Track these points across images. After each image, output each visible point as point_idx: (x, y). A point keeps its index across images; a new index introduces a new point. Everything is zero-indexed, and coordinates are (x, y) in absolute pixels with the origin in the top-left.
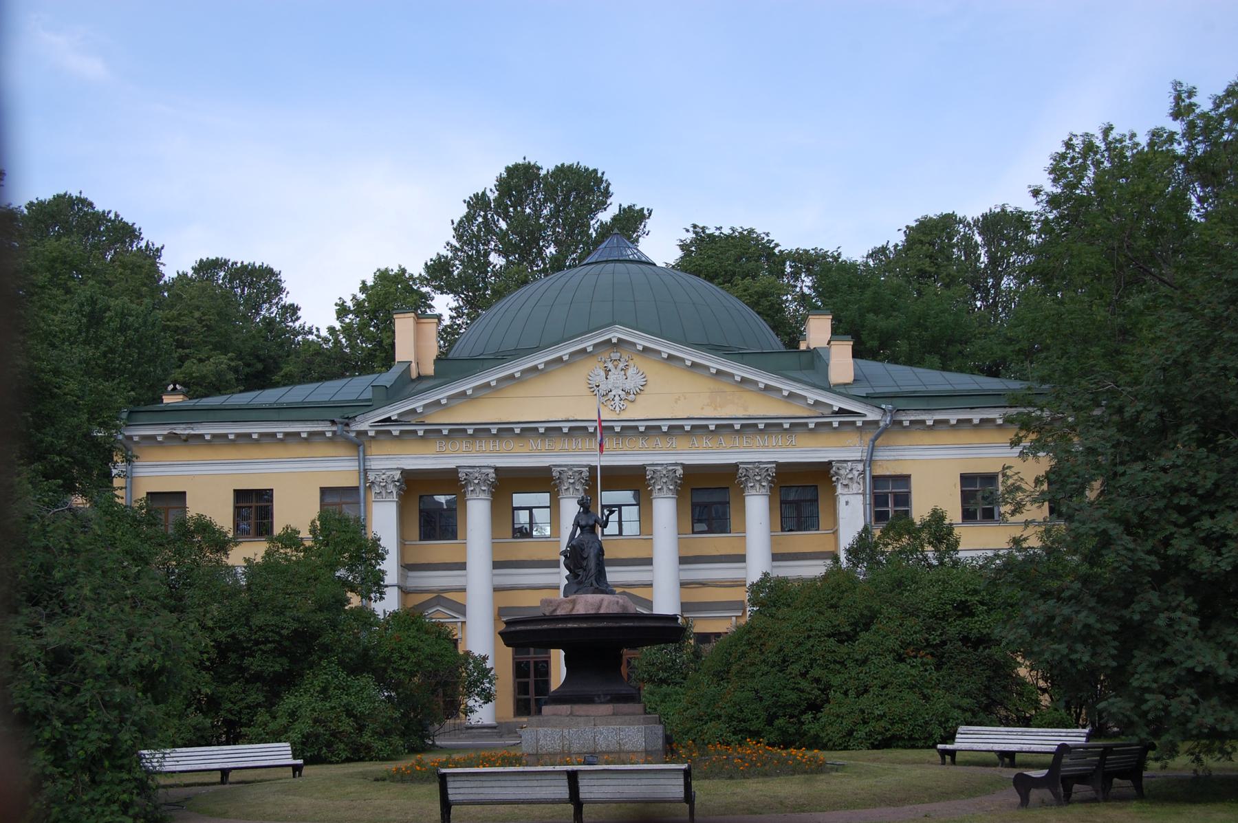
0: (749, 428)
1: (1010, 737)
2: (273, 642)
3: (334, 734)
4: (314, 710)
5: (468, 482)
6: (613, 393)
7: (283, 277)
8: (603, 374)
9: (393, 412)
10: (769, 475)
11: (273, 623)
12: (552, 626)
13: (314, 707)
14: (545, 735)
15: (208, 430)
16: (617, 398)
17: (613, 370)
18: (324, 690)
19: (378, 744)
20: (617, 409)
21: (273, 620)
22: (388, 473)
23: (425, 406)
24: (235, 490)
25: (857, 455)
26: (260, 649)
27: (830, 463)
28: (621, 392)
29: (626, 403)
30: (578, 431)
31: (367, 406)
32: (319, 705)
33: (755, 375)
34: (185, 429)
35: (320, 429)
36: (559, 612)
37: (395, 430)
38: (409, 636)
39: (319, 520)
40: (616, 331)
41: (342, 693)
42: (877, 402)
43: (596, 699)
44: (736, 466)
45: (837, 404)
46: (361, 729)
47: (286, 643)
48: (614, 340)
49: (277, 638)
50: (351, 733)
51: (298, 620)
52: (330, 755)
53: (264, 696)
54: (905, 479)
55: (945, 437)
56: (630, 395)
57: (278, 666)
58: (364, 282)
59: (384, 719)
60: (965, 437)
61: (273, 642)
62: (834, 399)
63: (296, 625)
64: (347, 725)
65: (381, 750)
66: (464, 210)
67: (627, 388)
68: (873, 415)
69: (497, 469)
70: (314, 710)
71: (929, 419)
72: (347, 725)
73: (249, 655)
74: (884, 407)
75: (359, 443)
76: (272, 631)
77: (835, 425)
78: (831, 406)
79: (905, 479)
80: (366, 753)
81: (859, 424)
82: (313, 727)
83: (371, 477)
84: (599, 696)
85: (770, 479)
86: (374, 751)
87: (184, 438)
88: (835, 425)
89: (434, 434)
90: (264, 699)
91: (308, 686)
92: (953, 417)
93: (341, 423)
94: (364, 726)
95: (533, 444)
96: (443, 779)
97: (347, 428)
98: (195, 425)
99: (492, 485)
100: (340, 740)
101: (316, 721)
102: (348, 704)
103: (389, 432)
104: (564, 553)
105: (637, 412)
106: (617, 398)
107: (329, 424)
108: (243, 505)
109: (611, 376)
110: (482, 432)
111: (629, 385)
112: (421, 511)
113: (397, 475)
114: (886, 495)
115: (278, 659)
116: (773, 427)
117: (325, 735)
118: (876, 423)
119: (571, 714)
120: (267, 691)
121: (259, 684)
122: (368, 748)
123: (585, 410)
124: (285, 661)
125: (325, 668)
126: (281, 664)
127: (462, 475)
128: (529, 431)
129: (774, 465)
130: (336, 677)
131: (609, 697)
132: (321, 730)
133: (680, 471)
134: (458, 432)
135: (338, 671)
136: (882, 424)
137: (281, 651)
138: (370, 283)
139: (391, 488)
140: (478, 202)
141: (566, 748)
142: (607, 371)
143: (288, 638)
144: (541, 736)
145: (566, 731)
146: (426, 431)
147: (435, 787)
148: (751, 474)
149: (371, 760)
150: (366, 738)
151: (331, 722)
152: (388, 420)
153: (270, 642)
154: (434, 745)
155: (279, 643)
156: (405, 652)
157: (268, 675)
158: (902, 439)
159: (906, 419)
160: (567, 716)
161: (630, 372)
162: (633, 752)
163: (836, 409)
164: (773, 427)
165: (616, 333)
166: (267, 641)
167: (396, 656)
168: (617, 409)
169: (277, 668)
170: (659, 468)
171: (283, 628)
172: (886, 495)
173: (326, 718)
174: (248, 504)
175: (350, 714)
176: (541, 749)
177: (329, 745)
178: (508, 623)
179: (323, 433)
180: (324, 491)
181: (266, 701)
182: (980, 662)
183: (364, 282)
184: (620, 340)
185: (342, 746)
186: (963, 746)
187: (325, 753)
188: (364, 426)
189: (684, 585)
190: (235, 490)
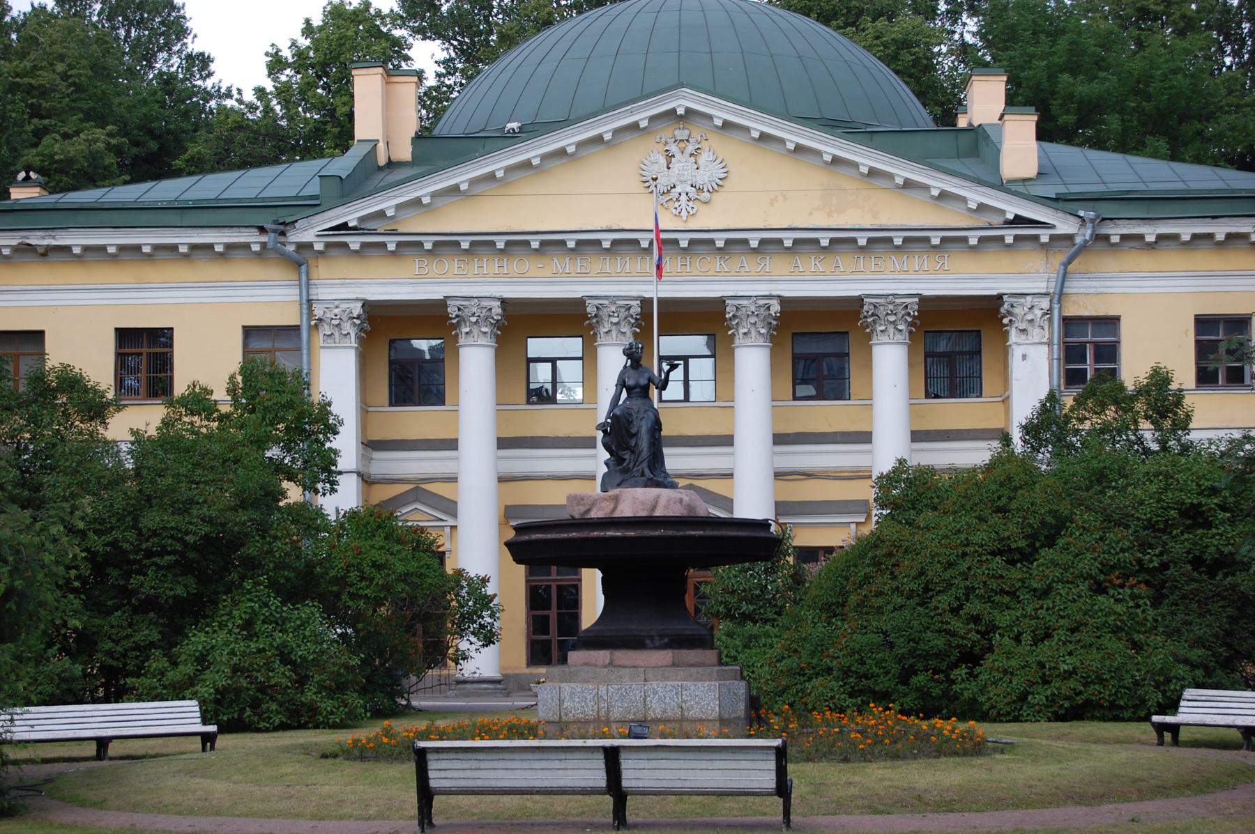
0: (879, 243)
2: (174, 552)
3: (262, 689)
4: (233, 653)
5: (461, 320)
6: (678, 189)
8: (663, 161)
9: (351, 214)
10: (909, 314)
11: (173, 524)
13: (233, 649)
14: (572, 695)
15: (76, 239)
17: (678, 155)
18: (248, 624)
19: (327, 705)
21: (173, 521)
22: (344, 306)
23: (399, 207)
25: (1041, 287)
27: (1000, 297)
28: (689, 189)
29: (697, 205)
31: (312, 206)
32: (240, 646)
34: (43, 238)
35: (242, 240)
36: (595, 514)
37: (354, 242)
40: (683, 98)
42: (1071, 206)
43: (648, 642)
44: (859, 300)
45: (1013, 208)
46: (302, 681)
48: (681, 111)
49: (179, 547)
51: (209, 521)
52: (256, 719)
54: (1112, 322)
56: (702, 193)
57: (180, 588)
58: (308, 22)
59: (336, 669)
60: (1203, 259)
61: (174, 552)
62: (1007, 202)
64: (281, 675)
65: (332, 713)
67: (699, 183)
68: (1065, 226)
70: (233, 653)
71: (1150, 232)
72: (281, 675)
74: (1082, 213)
76: (172, 537)
77: (1009, 240)
78: (1003, 212)
79: (1112, 322)
81: (1044, 239)
82: (231, 678)
83: (318, 311)
84: (652, 638)
85: (909, 319)
86: (321, 714)
87: (41, 250)
88: (1009, 240)
89: (410, 247)
91: (225, 618)
92: (1186, 230)
93: (274, 231)
94: (307, 677)
96: (421, 757)
97: (282, 239)
101: (236, 669)
102: (284, 645)
103: (345, 245)
104: (602, 427)
106: (684, 197)
107: (255, 232)
108: (127, 350)
109: (675, 164)
110: (482, 245)
111: (703, 178)
112: (391, 363)
113: (357, 309)
114: (1082, 346)
115: (180, 579)
116: (916, 242)
117: (248, 689)
118: (1070, 238)
119: (611, 664)
120: (163, 625)
121: (152, 615)
122: (313, 710)
125: (249, 592)
126: (186, 586)
127: (452, 311)
128: (552, 245)
129: (917, 300)
130: (266, 605)
132: (244, 683)
133: (776, 307)
134: (446, 246)
135: (269, 596)
136: (1078, 240)
137: (184, 567)
138: (317, 21)
139: (348, 327)
141: (602, 713)
142: (670, 157)
143: (195, 547)
144: (566, 695)
145: (603, 688)
147: (410, 769)
148: (881, 312)
149: (317, 727)
150: (309, 695)
151: (259, 671)
152: (344, 226)
153: (169, 553)
154: (409, 706)
155: (182, 554)
157: (166, 601)
158: (1107, 263)
159: (1115, 232)
160: (605, 667)
161: (704, 158)
162: (701, 720)
163: (1010, 216)
164: (916, 242)
165: (682, 101)
166: (163, 552)
167: (353, 575)
168: (684, 213)
169: (180, 591)
170: (745, 302)
171: (187, 533)
172: (1082, 346)
173: (251, 664)
176: (566, 714)
178: (518, 529)
179: (247, 246)
180: (249, 331)
183: (308, 22)
185: (274, 707)
190: (116, 329)
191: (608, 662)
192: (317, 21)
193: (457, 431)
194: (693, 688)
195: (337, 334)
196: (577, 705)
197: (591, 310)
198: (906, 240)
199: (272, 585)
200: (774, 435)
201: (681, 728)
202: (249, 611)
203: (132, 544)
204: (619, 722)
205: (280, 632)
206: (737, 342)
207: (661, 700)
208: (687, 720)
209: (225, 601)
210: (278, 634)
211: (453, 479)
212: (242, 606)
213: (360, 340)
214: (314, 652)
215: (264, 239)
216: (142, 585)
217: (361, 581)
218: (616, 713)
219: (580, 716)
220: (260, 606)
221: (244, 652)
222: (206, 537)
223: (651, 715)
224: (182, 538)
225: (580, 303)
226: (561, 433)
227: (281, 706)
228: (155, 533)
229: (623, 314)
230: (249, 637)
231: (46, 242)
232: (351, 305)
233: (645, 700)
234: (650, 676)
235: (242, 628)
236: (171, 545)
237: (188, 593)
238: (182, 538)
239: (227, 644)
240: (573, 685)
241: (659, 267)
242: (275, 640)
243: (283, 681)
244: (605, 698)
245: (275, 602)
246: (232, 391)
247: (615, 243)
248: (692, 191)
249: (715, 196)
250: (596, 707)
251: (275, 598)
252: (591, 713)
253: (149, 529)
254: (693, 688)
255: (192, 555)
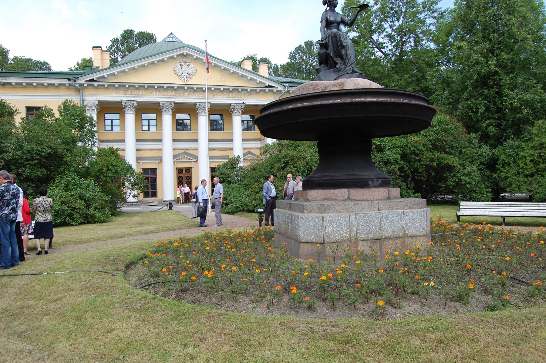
0: (236, 90)
1: (511, 208)
2: (36, 159)
3: (74, 209)
4: (61, 196)
5: (126, 107)
6: (184, 74)
7: (51, 65)
8: (180, 67)
11: (36, 149)
12: (347, 100)
13: (61, 195)
14: (332, 222)
15: (13, 80)
16: (185, 77)
17: (184, 66)
18: (67, 186)
19: (98, 214)
20: (185, 81)
21: (36, 148)
22: (93, 102)
23: (108, 75)
24: (26, 107)
26: (29, 164)
28: (187, 74)
29: (189, 79)
30: (171, 88)
32: (64, 194)
33: (239, 70)
34: (3, 80)
35: (63, 82)
37: (96, 84)
38: (111, 159)
39: (63, 105)
40: (186, 50)
41: (77, 188)
43: (370, 183)
45: (268, 83)
46: (88, 207)
47: (44, 160)
48: (185, 54)
49: (39, 157)
50: (83, 209)
51: (51, 147)
52: (71, 221)
53: (32, 189)
55: (52, 91)
57: (40, 173)
58: (78, 62)
59: (101, 201)
61: (36, 159)
62: (267, 81)
63: (50, 150)
64: (81, 204)
65: (100, 218)
66: (110, 43)
67: (189, 73)
68: (280, 88)
69: (138, 102)
70: (61, 196)
72: (81, 204)
73: (24, 167)
74: (284, 85)
75: (80, 89)
76: (36, 153)
78: (265, 84)
80: (92, 219)
81: (275, 91)
82: (61, 206)
84: (372, 180)
86: (96, 218)
87: (2, 83)
88: (267, 91)
89: (112, 86)
90: (32, 191)
91: (58, 184)
93: (73, 79)
94: (90, 204)
95: (152, 92)
97: (75, 82)
98: (7, 78)
99: (135, 108)
100: (77, 213)
101: (63, 203)
102: (81, 193)
103: (93, 85)
105: (194, 81)
106: (185, 77)
107: (67, 80)
108: (29, 113)
109: (183, 68)
110: (132, 87)
111: (190, 72)
113: (97, 103)
115: (40, 169)
116: (244, 90)
117: (68, 210)
118: (280, 91)
119: (349, 198)
120: (34, 187)
121: (29, 183)
122: (93, 216)
123: (175, 81)
124: (44, 170)
125: (67, 174)
126: (42, 172)
127: (123, 104)
128: (151, 87)
130: (74, 179)
131: (380, 181)
132: (66, 208)
134: (122, 86)
135: (75, 175)
136: (283, 92)
137: (41, 165)
138: (80, 62)
139: (94, 108)
140: (115, 41)
141: (353, 235)
143: (46, 158)
144: (327, 223)
145: (353, 217)
146: (108, 85)
148: (235, 108)
149: (95, 223)
150: (91, 211)
151: (72, 203)
152: (93, 80)
153: (35, 160)
154: (121, 212)
155: (40, 160)
156: (110, 167)
157: (34, 178)
160: (345, 201)
161: (190, 67)
162: (416, 236)
163: (267, 85)
164: (244, 90)
166: (32, 159)
167: (105, 169)
168: (185, 81)
169: (40, 174)
170: (201, 104)
171: (42, 152)
173: (69, 200)
174: (32, 113)
175: (81, 198)
176: (328, 237)
177: (70, 215)
179: (64, 85)
181: (34, 193)
182: (389, 172)
183: (78, 62)
184: (187, 54)
185: (78, 216)
186: (466, 213)
187: (68, 220)
188: (82, 82)
189: (210, 149)
190: (26, 107)
191: (346, 197)
192: (80, 62)
193: (125, 137)
194: (411, 214)
195: (91, 110)
196: (335, 230)
197: (161, 104)
198: (242, 90)
199: (76, 172)
200: (209, 139)
201: (404, 243)
202: (67, 181)
203: (20, 156)
204: (364, 240)
205: (80, 188)
206: (199, 114)
207: (391, 223)
208: (408, 236)
209: (58, 177)
210: (78, 189)
211: (124, 150)
212: (64, 179)
213: (98, 112)
214: (93, 195)
215: (69, 82)
216: (24, 172)
217: (108, 171)
218: (362, 235)
219: (338, 238)
220: (71, 179)
221: (66, 196)
222: (49, 154)
223: (385, 235)
224: (40, 154)
225: (158, 103)
226: (151, 138)
227: (80, 216)
228: (29, 152)
229: (170, 106)
230: (67, 190)
231: (3, 81)
232: (95, 102)
233: (381, 224)
234: (382, 206)
235: (64, 187)
236: (35, 156)
237: (43, 175)
238: (40, 154)
239: (58, 193)
240: (332, 215)
241: (208, 69)
242: (77, 191)
243: (81, 206)
244: (354, 223)
245: (77, 178)
246: (60, 111)
247: (168, 87)
248: (188, 75)
249: (193, 77)
250: (348, 230)
251: (77, 176)
252: (345, 236)
253: (26, 151)
254: (411, 214)
255: (44, 160)
